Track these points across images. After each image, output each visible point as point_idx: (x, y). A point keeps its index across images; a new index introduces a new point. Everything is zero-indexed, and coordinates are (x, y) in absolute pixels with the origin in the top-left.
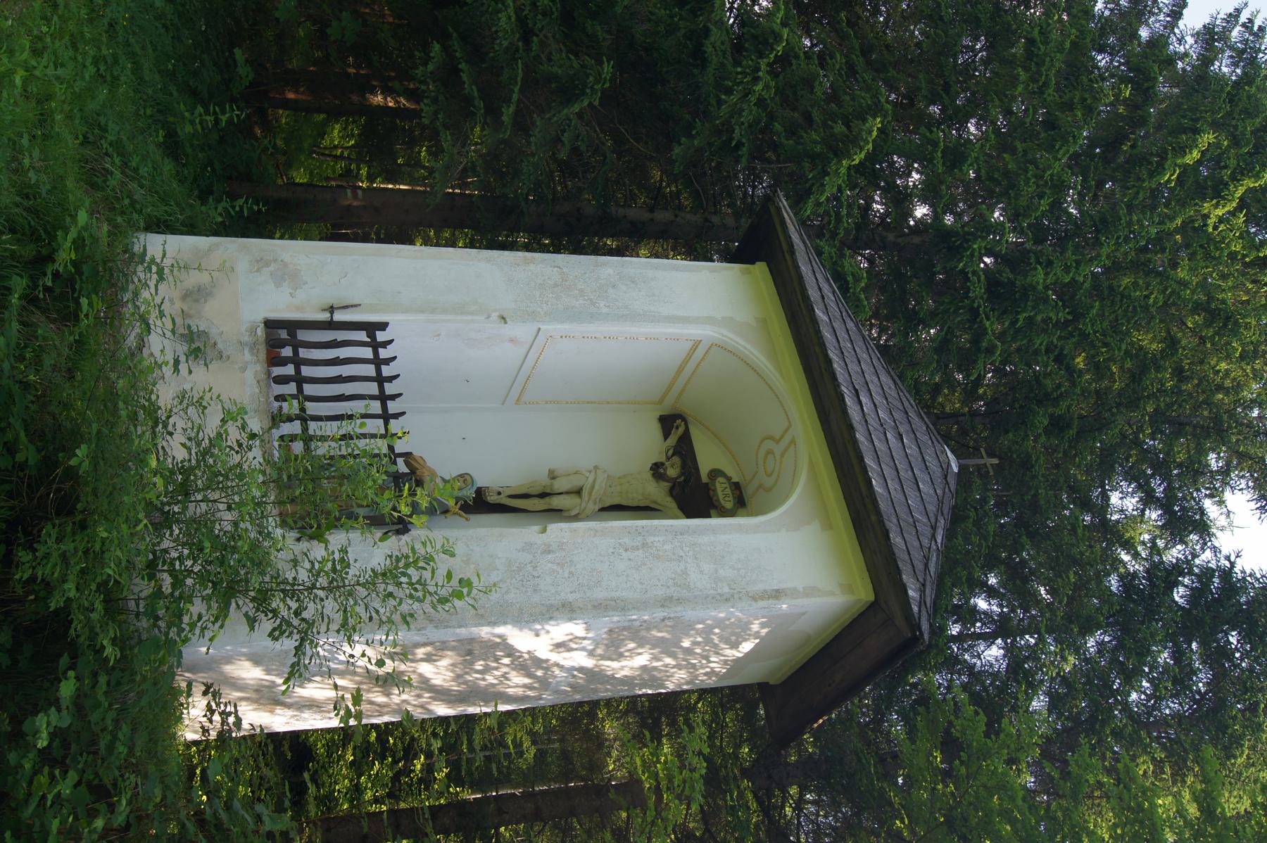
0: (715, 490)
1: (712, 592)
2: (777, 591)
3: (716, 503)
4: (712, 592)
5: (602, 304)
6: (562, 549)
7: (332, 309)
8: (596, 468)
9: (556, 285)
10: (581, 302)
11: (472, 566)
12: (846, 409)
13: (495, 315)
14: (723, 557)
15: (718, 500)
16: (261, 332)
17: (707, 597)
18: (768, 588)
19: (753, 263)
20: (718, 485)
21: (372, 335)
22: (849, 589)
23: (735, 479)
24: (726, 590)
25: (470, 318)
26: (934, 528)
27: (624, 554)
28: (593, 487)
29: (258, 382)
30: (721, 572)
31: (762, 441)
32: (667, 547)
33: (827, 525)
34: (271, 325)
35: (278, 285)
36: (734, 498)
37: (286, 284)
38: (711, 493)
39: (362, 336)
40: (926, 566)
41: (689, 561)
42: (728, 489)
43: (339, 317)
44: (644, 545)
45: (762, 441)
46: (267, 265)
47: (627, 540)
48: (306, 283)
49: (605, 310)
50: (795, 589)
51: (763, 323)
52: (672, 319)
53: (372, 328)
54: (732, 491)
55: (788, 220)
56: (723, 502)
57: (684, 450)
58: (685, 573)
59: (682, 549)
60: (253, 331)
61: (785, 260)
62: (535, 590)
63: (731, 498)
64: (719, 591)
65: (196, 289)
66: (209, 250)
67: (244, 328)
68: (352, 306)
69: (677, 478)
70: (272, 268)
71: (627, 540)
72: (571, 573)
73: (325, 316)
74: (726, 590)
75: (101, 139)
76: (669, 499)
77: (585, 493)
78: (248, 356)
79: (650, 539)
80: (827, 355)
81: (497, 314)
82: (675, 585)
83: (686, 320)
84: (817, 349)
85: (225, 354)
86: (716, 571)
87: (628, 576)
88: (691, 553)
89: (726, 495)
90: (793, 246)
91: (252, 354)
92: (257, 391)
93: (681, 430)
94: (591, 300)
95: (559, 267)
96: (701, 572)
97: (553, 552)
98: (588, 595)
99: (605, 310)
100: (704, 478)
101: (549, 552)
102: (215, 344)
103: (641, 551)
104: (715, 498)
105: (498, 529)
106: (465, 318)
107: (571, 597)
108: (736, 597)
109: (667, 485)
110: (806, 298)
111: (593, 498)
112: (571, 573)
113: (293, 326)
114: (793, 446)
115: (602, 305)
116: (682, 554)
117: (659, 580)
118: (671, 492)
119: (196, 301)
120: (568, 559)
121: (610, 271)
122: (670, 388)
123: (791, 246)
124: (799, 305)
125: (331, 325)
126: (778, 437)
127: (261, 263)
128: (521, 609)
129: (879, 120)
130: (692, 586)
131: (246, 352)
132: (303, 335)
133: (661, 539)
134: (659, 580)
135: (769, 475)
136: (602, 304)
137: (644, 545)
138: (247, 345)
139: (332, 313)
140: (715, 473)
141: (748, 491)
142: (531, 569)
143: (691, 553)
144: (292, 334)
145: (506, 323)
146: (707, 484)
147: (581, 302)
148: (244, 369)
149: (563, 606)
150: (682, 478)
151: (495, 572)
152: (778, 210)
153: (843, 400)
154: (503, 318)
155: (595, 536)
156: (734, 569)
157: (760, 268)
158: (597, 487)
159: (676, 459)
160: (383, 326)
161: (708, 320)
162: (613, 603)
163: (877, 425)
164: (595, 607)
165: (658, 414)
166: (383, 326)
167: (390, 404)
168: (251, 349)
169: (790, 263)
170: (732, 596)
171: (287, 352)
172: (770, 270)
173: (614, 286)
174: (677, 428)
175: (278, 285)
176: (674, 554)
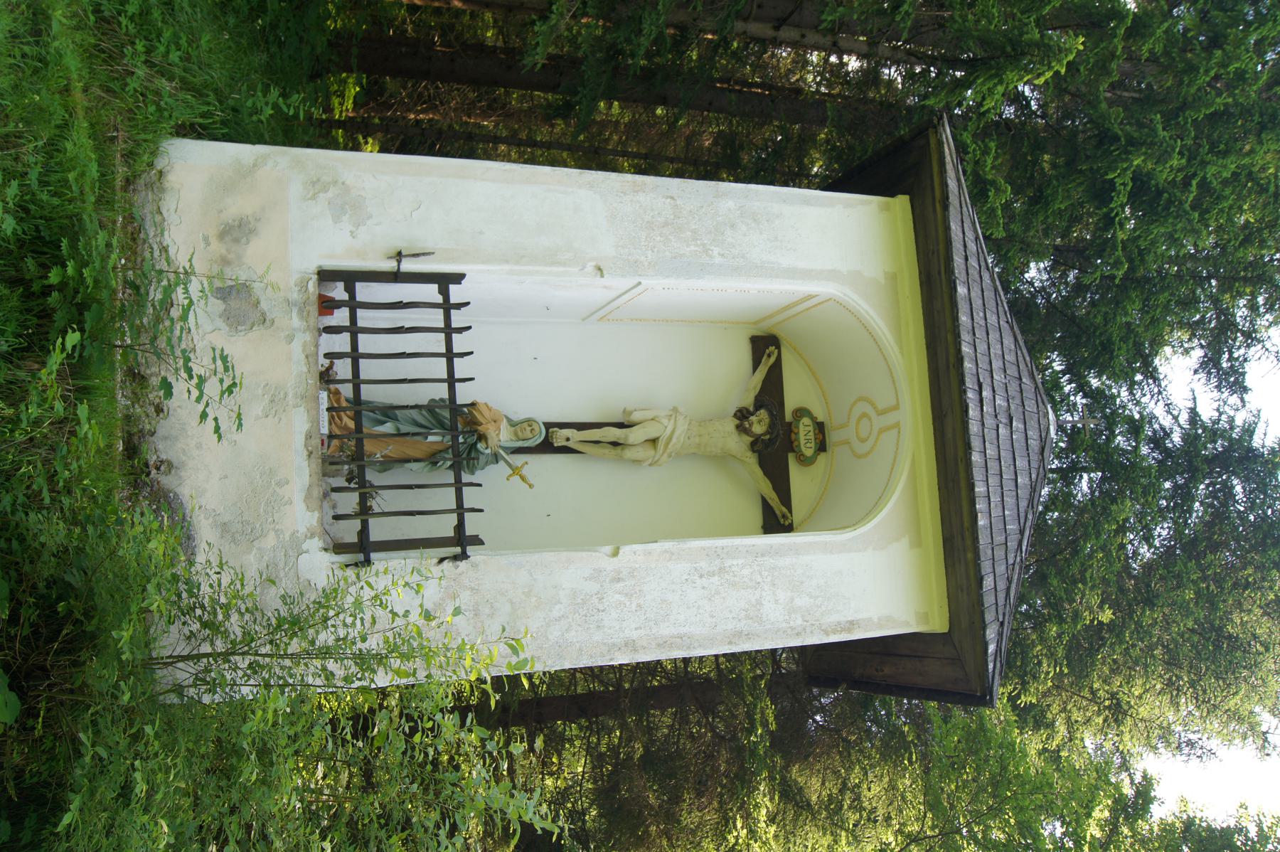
0: (797, 434)
2: (851, 623)
3: (796, 449)
4: (784, 625)
5: (716, 250)
6: (633, 576)
7: (399, 256)
8: (675, 410)
9: (666, 224)
10: (693, 248)
11: (534, 599)
12: (967, 423)
13: (590, 267)
14: (802, 583)
15: (799, 446)
16: (312, 286)
17: (778, 630)
18: (843, 619)
19: (892, 195)
20: (801, 426)
21: (444, 292)
22: (925, 617)
23: (820, 419)
24: (799, 622)
25: (561, 269)
26: (1022, 532)
27: (699, 581)
28: (670, 439)
29: (307, 357)
30: (799, 602)
31: (856, 402)
32: (746, 572)
33: (917, 542)
34: (326, 276)
35: (337, 219)
36: (816, 443)
37: (345, 218)
38: (793, 436)
39: (430, 292)
40: (1008, 589)
41: (766, 588)
42: (812, 433)
43: (408, 266)
44: (722, 570)
45: (856, 402)
46: (325, 189)
47: (704, 565)
48: (370, 217)
49: (718, 260)
50: (870, 619)
51: (893, 278)
52: (793, 273)
53: (445, 281)
55: (948, 159)
56: (803, 449)
57: (771, 393)
58: (759, 603)
59: (761, 575)
60: (303, 285)
61: (935, 211)
62: (598, 627)
63: (813, 445)
64: (792, 624)
65: (237, 223)
66: (255, 165)
67: (292, 283)
68: (424, 254)
69: (762, 435)
70: (330, 194)
71: (704, 565)
72: (639, 606)
73: (390, 265)
74: (799, 622)
75: (120, 14)
76: (749, 454)
77: (661, 444)
78: (296, 321)
79: (729, 563)
80: (959, 351)
81: (593, 263)
82: (748, 617)
83: (806, 275)
84: (950, 337)
85: (269, 316)
86: (792, 599)
87: (699, 608)
90: (947, 198)
92: (305, 369)
93: (773, 359)
94: (704, 245)
95: (672, 198)
96: (776, 601)
97: (623, 580)
98: (654, 631)
99: (718, 260)
100: (788, 417)
101: (619, 580)
102: (258, 303)
103: (716, 578)
104: (796, 444)
105: (565, 553)
106: (555, 269)
107: (635, 635)
108: (808, 630)
109: (750, 439)
110: (950, 270)
111: (668, 451)
112: (639, 606)
113: (350, 278)
114: (895, 431)
115: (715, 253)
116: (759, 580)
117: (731, 612)
118: (753, 446)
119: (237, 241)
120: (638, 588)
121: (731, 204)
122: (771, 316)
123: (946, 198)
124: (939, 273)
125: (396, 277)
126: (880, 407)
127: (316, 186)
128: (581, 650)
129: (1081, 39)
130: (764, 619)
131: (294, 315)
132: (365, 292)
133: (740, 561)
134: (731, 612)
135: (863, 441)
136: (716, 250)
137: (722, 570)
138: (296, 305)
139: (399, 262)
140: (801, 412)
141: (833, 437)
142: (597, 601)
143: (769, 578)
144: (350, 290)
145: (602, 276)
146: (790, 424)
147: (693, 248)
148: (290, 339)
149: (626, 645)
150: (768, 437)
151: (558, 607)
152: (940, 144)
153: (967, 411)
154: (600, 269)
155: (670, 559)
156: (811, 597)
157: (901, 203)
158: (674, 440)
159: (763, 413)
160: (458, 278)
161: (832, 275)
162: (679, 640)
163: (991, 410)
164: (659, 645)
166: (458, 278)
167: (453, 288)
168: (301, 311)
169: (939, 217)
170: (805, 629)
171: (341, 317)
173: (732, 226)
174: (769, 356)
175: (337, 219)
176: (751, 580)
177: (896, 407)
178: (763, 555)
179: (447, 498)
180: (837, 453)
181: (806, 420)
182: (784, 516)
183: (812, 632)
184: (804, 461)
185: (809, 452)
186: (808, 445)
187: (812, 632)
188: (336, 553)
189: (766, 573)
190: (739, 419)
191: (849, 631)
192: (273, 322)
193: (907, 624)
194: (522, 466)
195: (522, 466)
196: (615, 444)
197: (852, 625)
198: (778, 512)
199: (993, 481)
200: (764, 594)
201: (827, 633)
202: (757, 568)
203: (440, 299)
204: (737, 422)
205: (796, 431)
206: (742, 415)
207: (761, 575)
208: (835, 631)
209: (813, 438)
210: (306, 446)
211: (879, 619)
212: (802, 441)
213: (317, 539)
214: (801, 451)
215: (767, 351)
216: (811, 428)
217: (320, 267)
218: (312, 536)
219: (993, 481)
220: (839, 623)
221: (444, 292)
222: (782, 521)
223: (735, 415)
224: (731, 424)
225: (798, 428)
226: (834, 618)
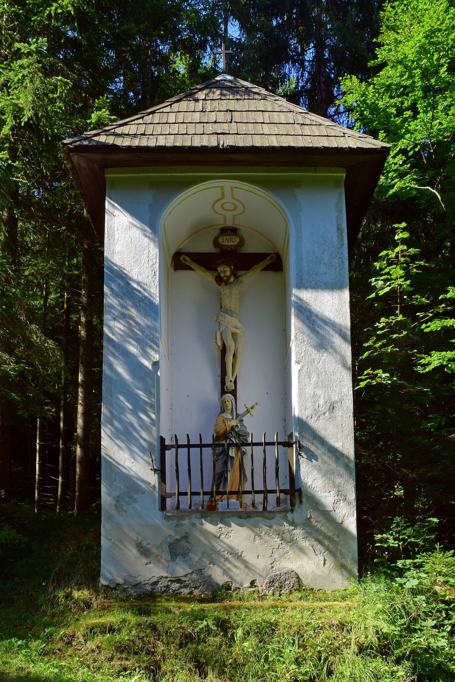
0: (228, 246)
1: (337, 270)
2: (338, 229)
4: (337, 270)
20: (224, 243)
22: (336, 183)
23: (219, 232)
24: (336, 261)
30: (326, 261)
35: (135, 501)
36: (232, 235)
38: (229, 249)
39: (170, 454)
42: (227, 237)
50: (337, 217)
53: (164, 447)
54: (228, 235)
56: (235, 243)
59: (311, 282)
63: (234, 237)
64: (337, 265)
86: (324, 264)
88: (314, 277)
89: (231, 240)
91: (185, 519)
93: (188, 259)
96: (325, 273)
104: (233, 248)
108: (341, 256)
116: (314, 282)
134: (329, 300)
140: (216, 243)
146: (222, 250)
150: (232, 267)
160: (162, 440)
165: (173, 271)
167: (167, 443)
170: (340, 258)
172: (303, 166)
174: (185, 260)
177: (222, 188)
178: (302, 280)
179: (258, 450)
180: (240, 222)
181: (220, 240)
182: (272, 258)
183: (342, 254)
184: (242, 243)
185: (237, 241)
186: (234, 240)
187: (342, 254)
188: (295, 505)
189: (311, 278)
190: (221, 283)
191: (342, 231)
192: (186, 533)
193: (340, 194)
194: (246, 407)
195: (246, 407)
196: (234, 356)
197: (339, 229)
198: (269, 262)
199: (266, 129)
200: (321, 280)
201: (342, 245)
202: (308, 284)
203: (174, 450)
204: (223, 284)
205: (226, 247)
206: (219, 280)
207: (311, 282)
208: (342, 240)
209: (229, 237)
210: (245, 518)
211: (337, 212)
212: (231, 244)
213: (288, 514)
214: (237, 245)
215: (183, 261)
216: (225, 237)
217: (159, 509)
218: (286, 516)
219: (266, 129)
220: (338, 237)
221: (169, 448)
222: (274, 260)
223: (220, 285)
224: (225, 290)
225: (224, 245)
226: (335, 239)
